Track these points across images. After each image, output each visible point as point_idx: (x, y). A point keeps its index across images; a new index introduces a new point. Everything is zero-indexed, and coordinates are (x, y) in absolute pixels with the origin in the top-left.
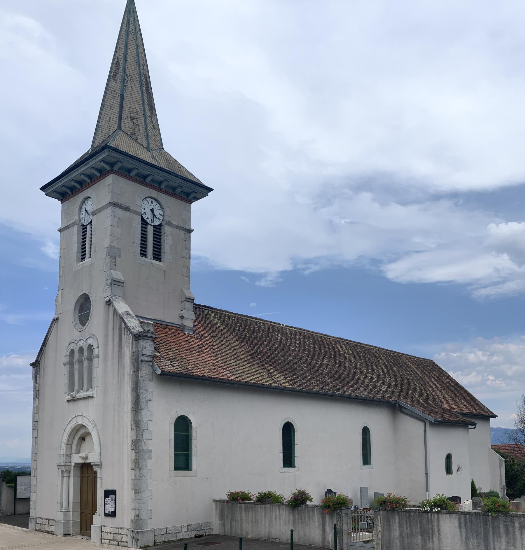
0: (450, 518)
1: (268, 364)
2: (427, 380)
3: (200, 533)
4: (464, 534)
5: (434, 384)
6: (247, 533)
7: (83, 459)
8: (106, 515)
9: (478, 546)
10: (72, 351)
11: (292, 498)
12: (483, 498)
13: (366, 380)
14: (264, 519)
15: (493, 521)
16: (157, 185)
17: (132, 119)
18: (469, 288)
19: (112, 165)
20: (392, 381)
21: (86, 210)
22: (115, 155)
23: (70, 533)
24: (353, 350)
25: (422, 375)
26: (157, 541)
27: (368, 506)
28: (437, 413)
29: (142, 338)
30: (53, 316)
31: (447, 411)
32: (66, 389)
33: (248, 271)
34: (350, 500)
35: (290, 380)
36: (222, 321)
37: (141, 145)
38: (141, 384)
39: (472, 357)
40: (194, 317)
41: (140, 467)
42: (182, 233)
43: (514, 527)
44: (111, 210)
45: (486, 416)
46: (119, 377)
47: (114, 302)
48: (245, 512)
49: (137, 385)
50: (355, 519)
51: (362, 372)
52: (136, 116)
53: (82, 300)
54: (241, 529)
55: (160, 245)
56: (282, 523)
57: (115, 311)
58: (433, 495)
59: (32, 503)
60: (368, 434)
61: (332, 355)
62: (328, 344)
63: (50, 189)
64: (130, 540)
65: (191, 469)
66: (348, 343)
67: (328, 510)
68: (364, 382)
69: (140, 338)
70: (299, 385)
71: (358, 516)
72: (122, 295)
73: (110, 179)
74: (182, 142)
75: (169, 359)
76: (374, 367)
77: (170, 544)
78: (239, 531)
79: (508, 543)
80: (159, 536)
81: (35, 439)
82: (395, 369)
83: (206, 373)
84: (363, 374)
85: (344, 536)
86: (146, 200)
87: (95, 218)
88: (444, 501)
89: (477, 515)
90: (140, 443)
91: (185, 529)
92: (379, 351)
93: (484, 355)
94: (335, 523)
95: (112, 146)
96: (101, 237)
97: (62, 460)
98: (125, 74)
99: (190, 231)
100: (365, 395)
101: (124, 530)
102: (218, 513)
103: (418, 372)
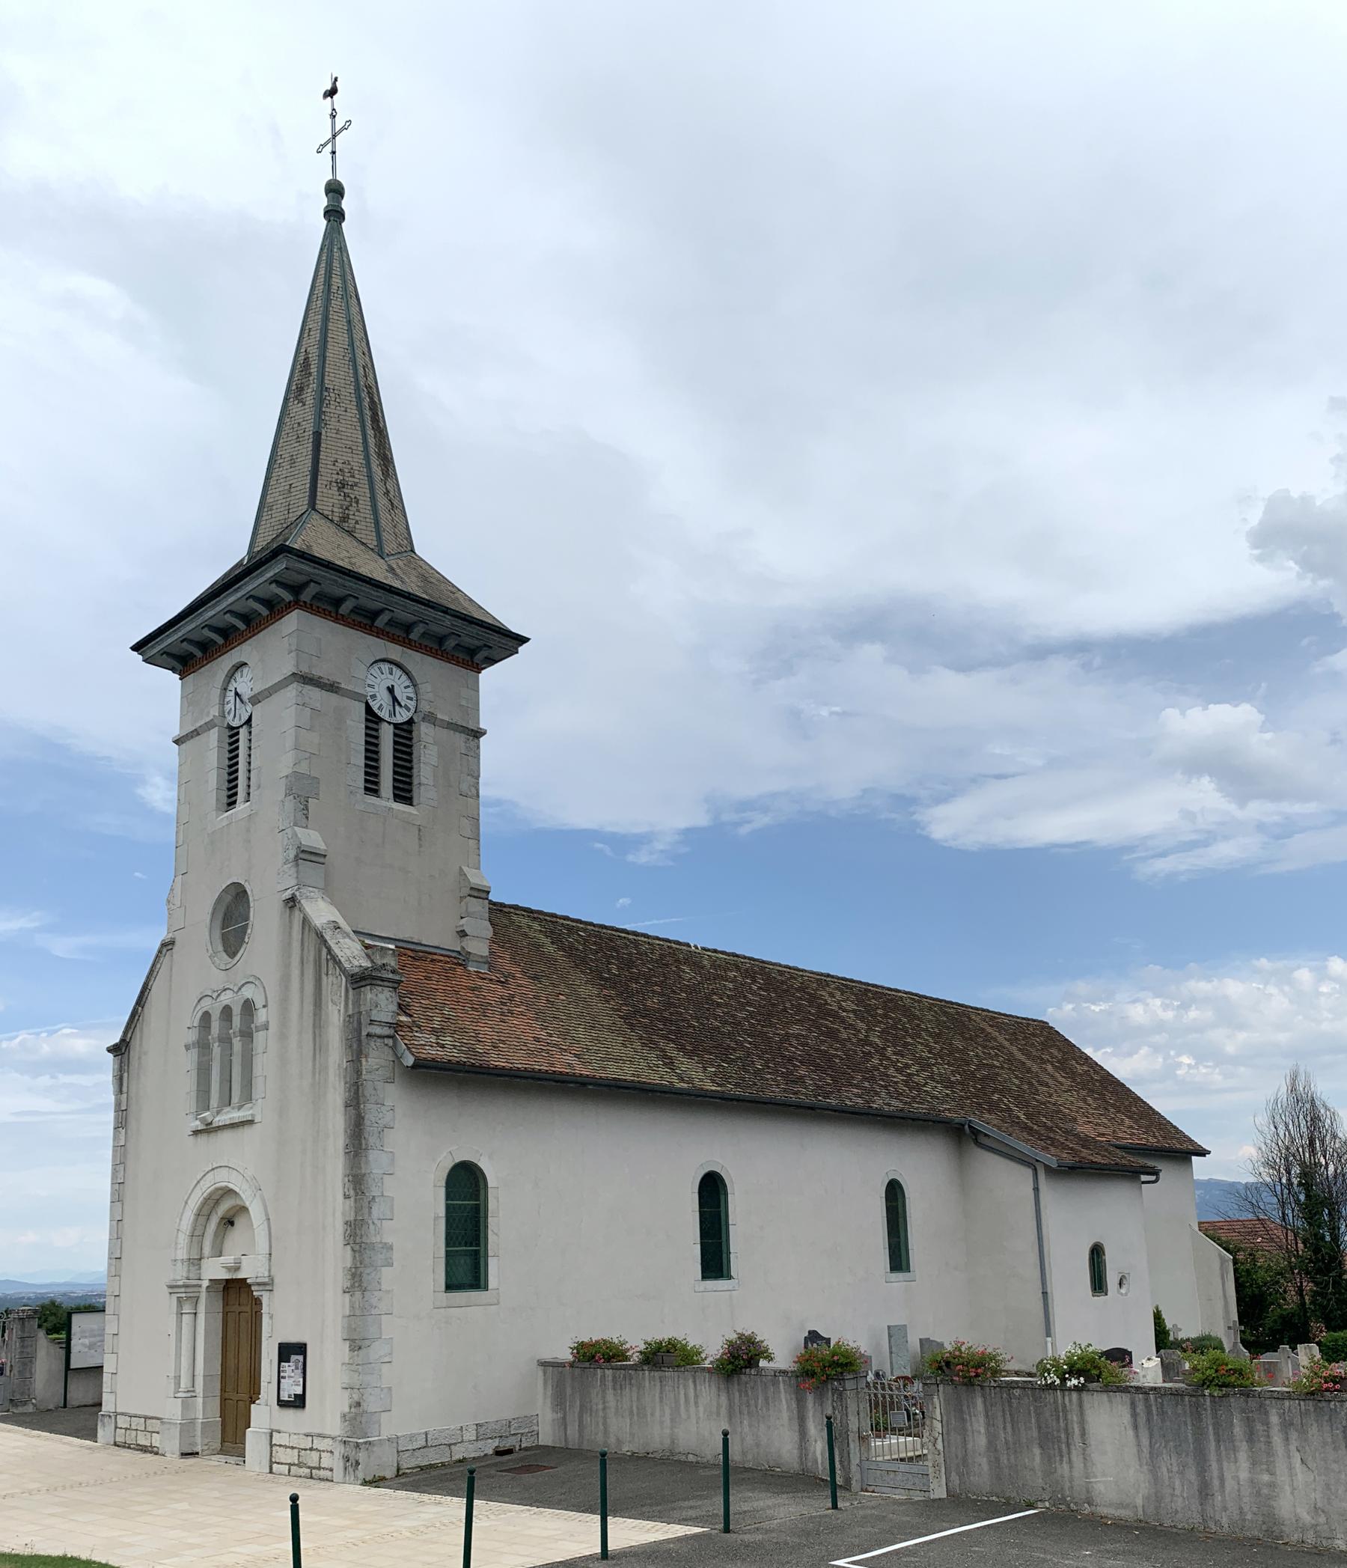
0: (1110, 1401)
2: (1035, 1068)
3: (506, 1444)
4: (1145, 1442)
6: (619, 1442)
7: (229, 1269)
8: (282, 1404)
9: (1181, 1473)
10: (206, 1016)
11: (724, 1354)
12: (1189, 1352)
13: (891, 1071)
15: (1215, 1411)
16: (400, 633)
17: (342, 486)
18: (1125, 858)
19: (296, 589)
21: (237, 694)
23: (195, 1450)
24: (859, 1002)
25: (1023, 1058)
26: (404, 1465)
27: (908, 1373)
31: (1085, 1142)
33: (609, 829)
34: (862, 1355)
37: (363, 544)
38: (368, 1090)
39: (1137, 1013)
40: (488, 931)
42: (459, 739)
43: (1267, 1424)
44: (294, 693)
45: (1182, 1151)
46: (314, 1074)
49: (357, 1092)
53: (229, 898)
54: (606, 1432)
55: (411, 769)
57: (306, 921)
58: (1064, 1346)
59: (106, 1378)
60: (899, 1196)
62: (801, 989)
65: (486, 1288)
66: (846, 985)
67: (811, 1382)
68: (887, 1076)
70: (737, 1085)
71: (884, 1396)
72: (321, 885)
73: (293, 620)
74: (455, 537)
75: (434, 1031)
76: (909, 1040)
77: (433, 1473)
78: (600, 1438)
79: (1254, 1463)
80: (407, 1454)
81: (118, 1223)
82: (958, 1043)
83: (519, 1061)
84: (883, 1056)
85: (852, 1446)
86: (376, 667)
87: (258, 713)
88: (1092, 1361)
89: (1176, 1394)
90: (365, 1227)
91: (470, 1435)
92: (919, 1002)
93: (1165, 1007)
94: (829, 1412)
95: (296, 546)
96: (272, 758)
97: (180, 1274)
98: (322, 387)
99: (478, 734)
100: (889, 1105)
102: (549, 1393)
103: (1014, 1050)
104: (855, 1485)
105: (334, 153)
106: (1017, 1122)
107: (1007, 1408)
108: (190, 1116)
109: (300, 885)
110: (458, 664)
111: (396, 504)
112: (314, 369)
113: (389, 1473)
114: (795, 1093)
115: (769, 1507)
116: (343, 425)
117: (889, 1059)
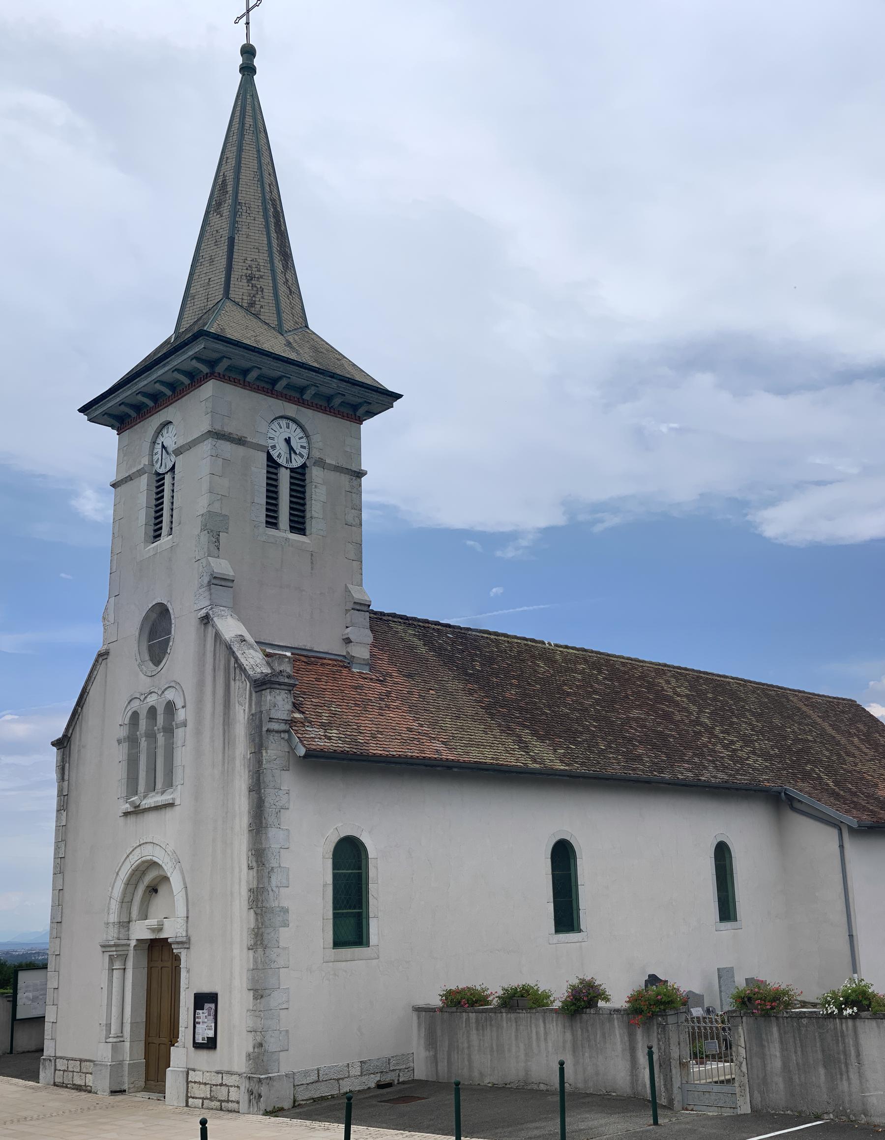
0: (878, 1027)
1: (519, 724)
2: (843, 741)
3: (387, 1078)
5: (858, 748)
6: (481, 1074)
7: (153, 930)
8: (197, 1046)
10: (135, 716)
11: (568, 997)
13: (718, 747)
14: (514, 1042)
16: (296, 395)
17: (250, 278)
19: (212, 364)
20: (772, 747)
21: (163, 446)
22: (217, 346)
24: (692, 687)
25: (833, 733)
28: (864, 809)
29: (268, 686)
30: (100, 647)
32: (122, 790)
35: (564, 755)
36: (428, 642)
38: (268, 778)
40: (369, 637)
41: (265, 943)
42: (345, 479)
47: (215, 619)
48: (477, 1029)
49: (258, 779)
50: (693, 1033)
51: (710, 731)
52: (257, 274)
53: (154, 616)
55: (304, 505)
56: (550, 1049)
57: (217, 636)
59: (48, 1026)
60: (727, 856)
61: (648, 698)
62: (641, 678)
63: (98, 411)
64: (244, 1098)
65: (368, 945)
66: (680, 673)
67: (639, 1018)
68: (715, 752)
69: (264, 687)
71: (705, 1028)
73: (209, 389)
74: (344, 309)
75: (322, 725)
76: (735, 720)
77: (325, 1104)
80: (302, 1088)
81: (59, 892)
83: (394, 749)
84: (712, 735)
85: (674, 1071)
86: (276, 423)
87: (181, 462)
90: (265, 894)
91: (355, 1071)
92: (744, 686)
96: (191, 498)
97: (112, 935)
98: (236, 202)
99: (360, 474)
100: (715, 777)
101: (234, 1077)
102: (423, 1035)
103: (826, 725)
104: (677, 1105)
105: (248, 23)
106: (826, 789)
107: (797, 1035)
108: (121, 801)
109: (213, 605)
110: (343, 417)
111: (294, 290)
112: (230, 188)
113: (287, 1105)
114: (634, 770)
115: (601, 1126)
116: (253, 233)
117: (716, 737)
